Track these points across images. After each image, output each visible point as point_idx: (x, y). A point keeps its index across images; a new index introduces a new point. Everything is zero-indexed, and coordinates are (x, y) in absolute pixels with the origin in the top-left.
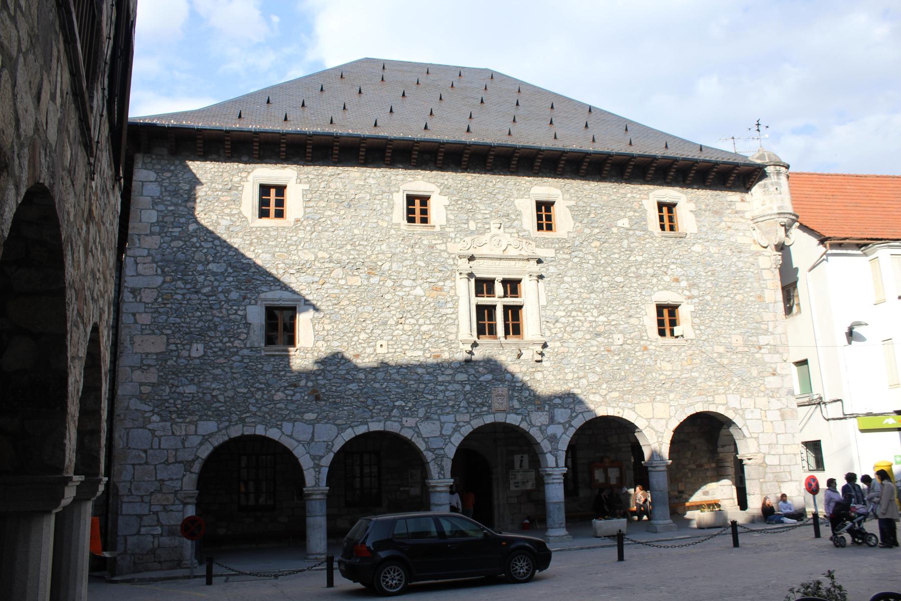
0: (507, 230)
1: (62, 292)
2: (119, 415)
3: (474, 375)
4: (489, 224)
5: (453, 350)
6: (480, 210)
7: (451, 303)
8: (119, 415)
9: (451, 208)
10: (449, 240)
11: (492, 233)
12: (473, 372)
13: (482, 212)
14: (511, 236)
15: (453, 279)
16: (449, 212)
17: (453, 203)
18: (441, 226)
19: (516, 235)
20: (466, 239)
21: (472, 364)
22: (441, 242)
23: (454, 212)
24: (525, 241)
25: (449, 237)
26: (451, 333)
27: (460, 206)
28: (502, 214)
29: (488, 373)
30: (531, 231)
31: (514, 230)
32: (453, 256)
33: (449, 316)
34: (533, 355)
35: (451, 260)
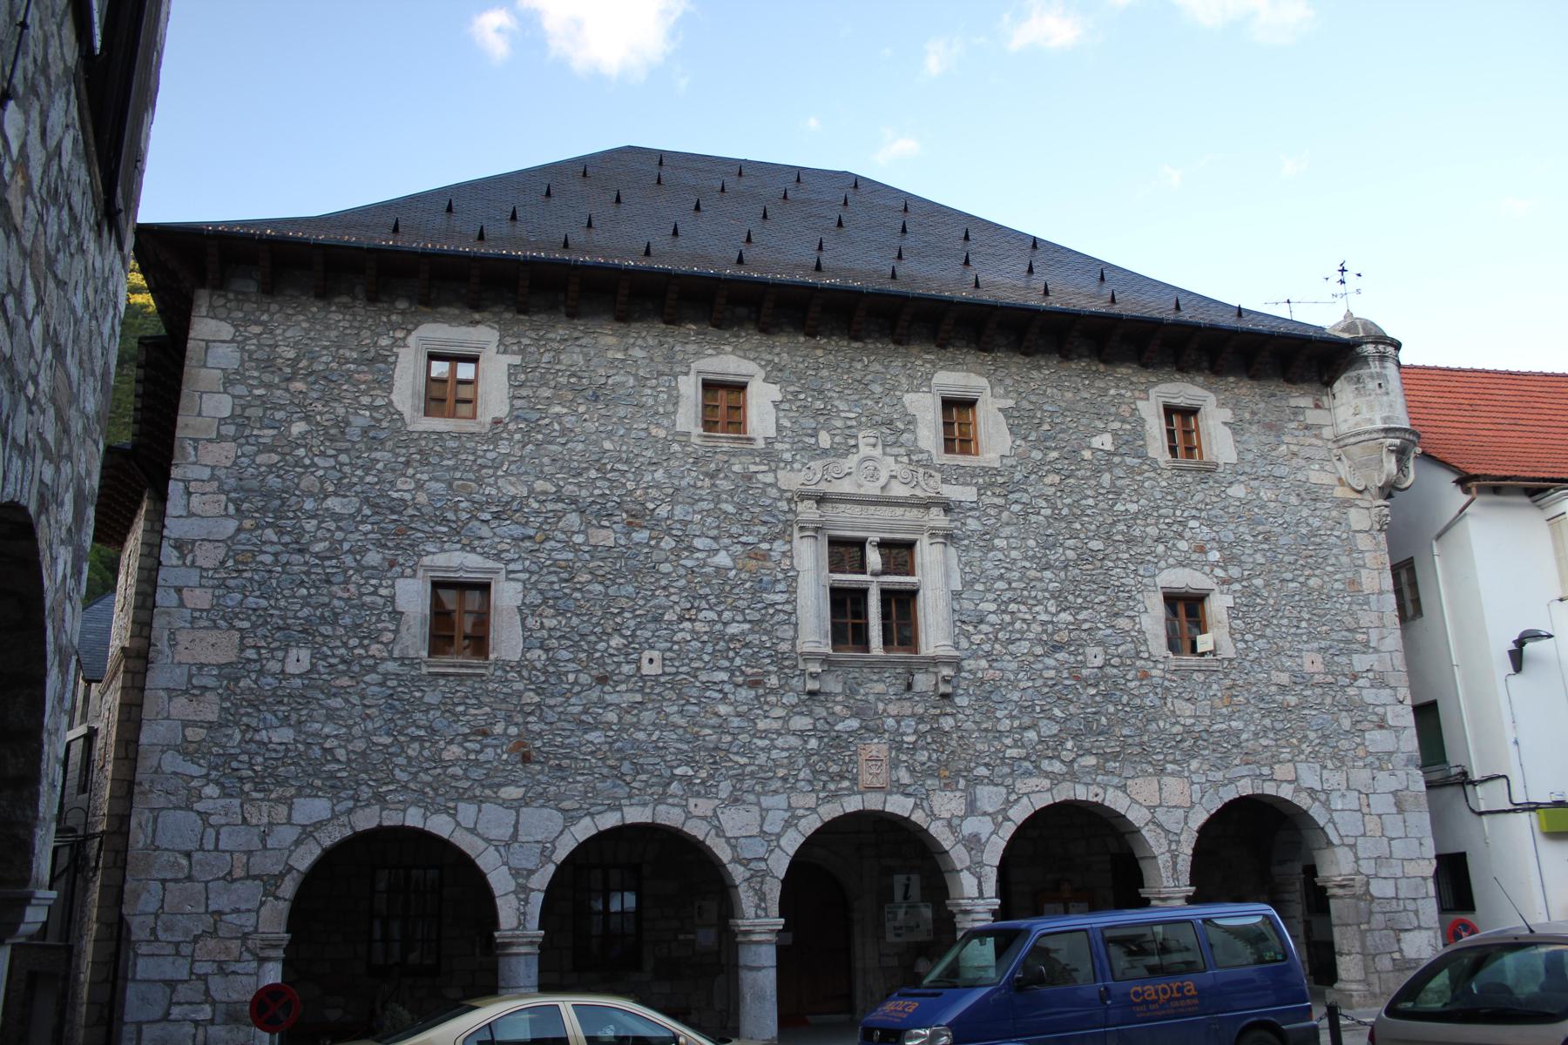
0: (888, 450)
4: (856, 437)
5: (786, 671)
6: (839, 411)
7: (783, 583)
9: (786, 406)
10: (782, 465)
12: (825, 714)
13: (843, 415)
16: (781, 414)
17: (790, 397)
18: (766, 438)
19: (905, 459)
20: (812, 464)
21: (822, 698)
25: (781, 460)
29: (852, 716)
30: (934, 452)
31: (902, 451)
32: (789, 495)
34: (936, 684)
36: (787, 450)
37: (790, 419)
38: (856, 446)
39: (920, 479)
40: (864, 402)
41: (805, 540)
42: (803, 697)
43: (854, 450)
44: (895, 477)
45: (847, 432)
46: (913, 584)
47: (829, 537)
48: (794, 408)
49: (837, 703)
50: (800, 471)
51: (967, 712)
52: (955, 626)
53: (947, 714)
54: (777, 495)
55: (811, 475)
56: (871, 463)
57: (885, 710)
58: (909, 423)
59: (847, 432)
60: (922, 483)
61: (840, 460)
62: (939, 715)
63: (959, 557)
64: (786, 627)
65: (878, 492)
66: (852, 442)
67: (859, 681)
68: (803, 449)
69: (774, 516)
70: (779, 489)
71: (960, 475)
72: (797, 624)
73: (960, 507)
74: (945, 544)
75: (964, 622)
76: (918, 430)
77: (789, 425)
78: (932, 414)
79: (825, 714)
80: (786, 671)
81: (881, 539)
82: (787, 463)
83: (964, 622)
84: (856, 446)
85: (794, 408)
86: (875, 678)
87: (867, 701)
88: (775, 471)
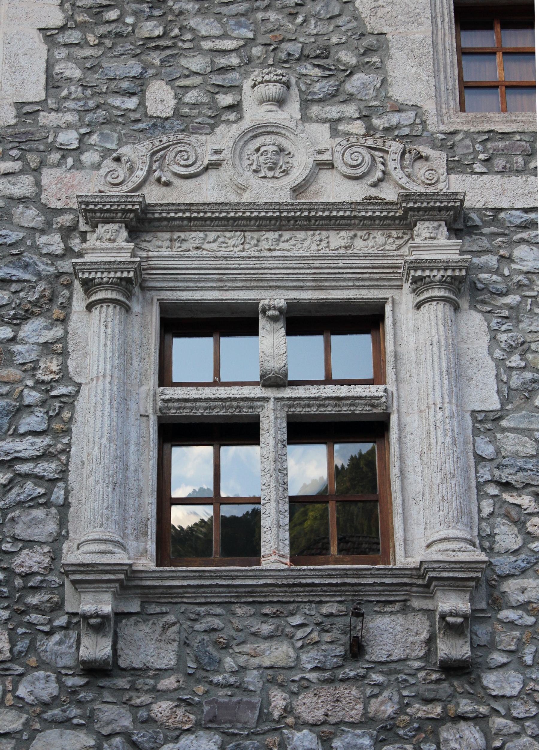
0: (315, 110)
1: (290, 557)
2: (398, 619)
3: (126, 735)
4: (237, 88)
5: (34, 617)
6: (197, 38)
7: (40, 412)
8: (398, 619)
9: (74, 36)
10: (55, 157)
11: (246, 123)
12: (127, 722)
13: (207, 45)
14: (334, 133)
15: (57, 313)
16: (61, 53)
17: (80, 18)
18: (19, 105)
19: (358, 127)
20: (126, 151)
21: (122, 682)
22: (17, 166)
23: (87, 52)
24: (396, 147)
25: (52, 148)
26: (29, 543)
27: (111, 28)
28: (295, 48)
29: (198, 726)
30: (429, 106)
31: (350, 110)
32: (66, 219)
33: (24, 468)
34: (431, 641)
35: (56, 238)
36: (69, 126)
37: (79, 62)
38: (235, 107)
39: (391, 165)
40: (260, 15)
41: (96, 311)
42: (70, 682)
43: (232, 116)
44: (330, 165)
45: (217, 79)
46: (372, 400)
47: (164, 307)
48: (92, 39)
49: (162, 694)
50: (97, 167)
51: (519, 711)
52: (481, 495)
53: (463, 718)
54: (39, 221)
55: (121, 172)
56: (267, 139)
57: (288, 710)
58: (368, 51)
59: (217, 79)
60: (397, 175)
61: (193, 139)
62: (440, 721)
63: (493, 334)
64: (39, 513)
65: (285, 197)
66: (226, 100)
67: (223, 637)
68: (107, 122)
69: (26, 266)
70: (44, 209)
71: (498, 153)
72: (66, 505)
73: (495, 220)
74: (457, 308)
75: (506, 486)
76: (390, 66)
77: (77, 73)
78: (426, 28)
79: (127, 722)
80: (34, 617)
81: (292, 305)
82: (65, 152)
83: (506, 486)
84: (235, 107)
85: (92, 39)
86: (266, 628)
87: (241, 687)
88: (37, 171)
